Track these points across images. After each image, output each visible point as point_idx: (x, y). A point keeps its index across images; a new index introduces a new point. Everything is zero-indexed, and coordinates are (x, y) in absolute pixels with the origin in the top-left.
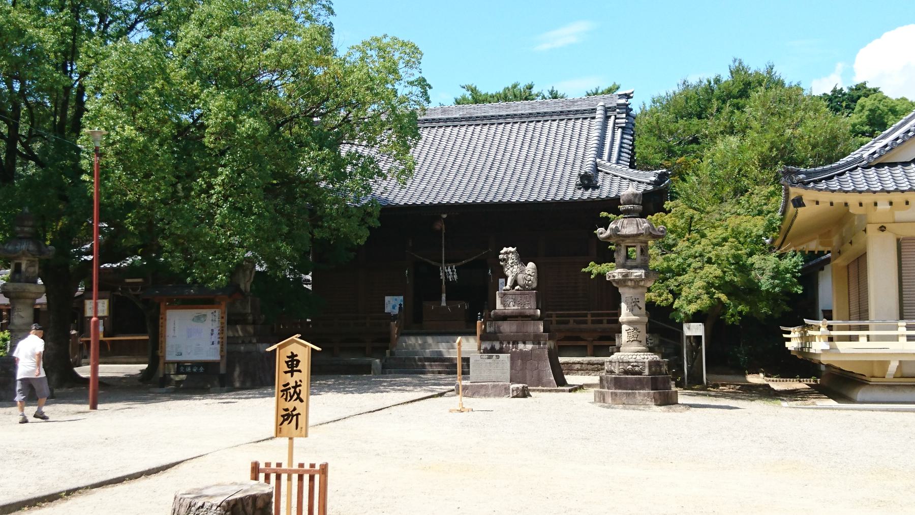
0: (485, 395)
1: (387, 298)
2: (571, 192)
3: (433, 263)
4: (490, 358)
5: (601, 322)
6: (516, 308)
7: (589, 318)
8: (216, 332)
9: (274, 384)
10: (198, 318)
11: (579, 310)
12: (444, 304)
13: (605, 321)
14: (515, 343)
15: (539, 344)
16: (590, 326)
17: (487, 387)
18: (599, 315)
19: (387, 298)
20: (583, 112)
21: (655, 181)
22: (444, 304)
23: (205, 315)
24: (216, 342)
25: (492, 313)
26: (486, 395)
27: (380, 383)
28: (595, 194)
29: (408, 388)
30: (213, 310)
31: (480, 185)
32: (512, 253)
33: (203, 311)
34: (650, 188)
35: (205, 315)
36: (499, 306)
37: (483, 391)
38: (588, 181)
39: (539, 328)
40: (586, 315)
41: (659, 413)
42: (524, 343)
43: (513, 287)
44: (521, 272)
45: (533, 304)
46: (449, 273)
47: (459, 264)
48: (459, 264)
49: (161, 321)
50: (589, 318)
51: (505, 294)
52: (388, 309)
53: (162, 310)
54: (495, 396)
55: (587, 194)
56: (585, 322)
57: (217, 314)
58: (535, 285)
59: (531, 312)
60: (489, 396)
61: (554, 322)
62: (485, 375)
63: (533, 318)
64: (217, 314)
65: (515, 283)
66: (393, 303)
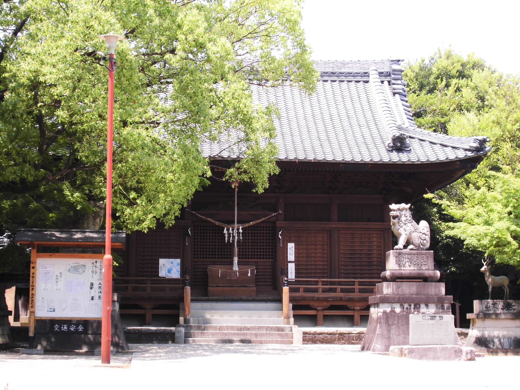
0: (434, 359)
1: (162, 261)
3: (217, 223)
6: (412, 268)
7: (357, 287)
8: (96, 286)
10: (75, 269)
12: (236, 268)
16: (320, 295)
17: (435, 350)
18: (331, 283)
19: (162, 261)
22: (236, 268)
24: (96, 298)
29: (207, 353)
30: (94, 261)
31: (350, 137)
34: (470, 154)
37: (431, 354)
38: (399, 144)
43: (405, 247)
44: (416, 230)
45: (431, 263)
49: (32, 271)
50: (357, 287)
54: (445, 359)
55: (395, 157)
58: (428, 245)
61: (356, 290)
65: (408, 243)
66: (168, 266)
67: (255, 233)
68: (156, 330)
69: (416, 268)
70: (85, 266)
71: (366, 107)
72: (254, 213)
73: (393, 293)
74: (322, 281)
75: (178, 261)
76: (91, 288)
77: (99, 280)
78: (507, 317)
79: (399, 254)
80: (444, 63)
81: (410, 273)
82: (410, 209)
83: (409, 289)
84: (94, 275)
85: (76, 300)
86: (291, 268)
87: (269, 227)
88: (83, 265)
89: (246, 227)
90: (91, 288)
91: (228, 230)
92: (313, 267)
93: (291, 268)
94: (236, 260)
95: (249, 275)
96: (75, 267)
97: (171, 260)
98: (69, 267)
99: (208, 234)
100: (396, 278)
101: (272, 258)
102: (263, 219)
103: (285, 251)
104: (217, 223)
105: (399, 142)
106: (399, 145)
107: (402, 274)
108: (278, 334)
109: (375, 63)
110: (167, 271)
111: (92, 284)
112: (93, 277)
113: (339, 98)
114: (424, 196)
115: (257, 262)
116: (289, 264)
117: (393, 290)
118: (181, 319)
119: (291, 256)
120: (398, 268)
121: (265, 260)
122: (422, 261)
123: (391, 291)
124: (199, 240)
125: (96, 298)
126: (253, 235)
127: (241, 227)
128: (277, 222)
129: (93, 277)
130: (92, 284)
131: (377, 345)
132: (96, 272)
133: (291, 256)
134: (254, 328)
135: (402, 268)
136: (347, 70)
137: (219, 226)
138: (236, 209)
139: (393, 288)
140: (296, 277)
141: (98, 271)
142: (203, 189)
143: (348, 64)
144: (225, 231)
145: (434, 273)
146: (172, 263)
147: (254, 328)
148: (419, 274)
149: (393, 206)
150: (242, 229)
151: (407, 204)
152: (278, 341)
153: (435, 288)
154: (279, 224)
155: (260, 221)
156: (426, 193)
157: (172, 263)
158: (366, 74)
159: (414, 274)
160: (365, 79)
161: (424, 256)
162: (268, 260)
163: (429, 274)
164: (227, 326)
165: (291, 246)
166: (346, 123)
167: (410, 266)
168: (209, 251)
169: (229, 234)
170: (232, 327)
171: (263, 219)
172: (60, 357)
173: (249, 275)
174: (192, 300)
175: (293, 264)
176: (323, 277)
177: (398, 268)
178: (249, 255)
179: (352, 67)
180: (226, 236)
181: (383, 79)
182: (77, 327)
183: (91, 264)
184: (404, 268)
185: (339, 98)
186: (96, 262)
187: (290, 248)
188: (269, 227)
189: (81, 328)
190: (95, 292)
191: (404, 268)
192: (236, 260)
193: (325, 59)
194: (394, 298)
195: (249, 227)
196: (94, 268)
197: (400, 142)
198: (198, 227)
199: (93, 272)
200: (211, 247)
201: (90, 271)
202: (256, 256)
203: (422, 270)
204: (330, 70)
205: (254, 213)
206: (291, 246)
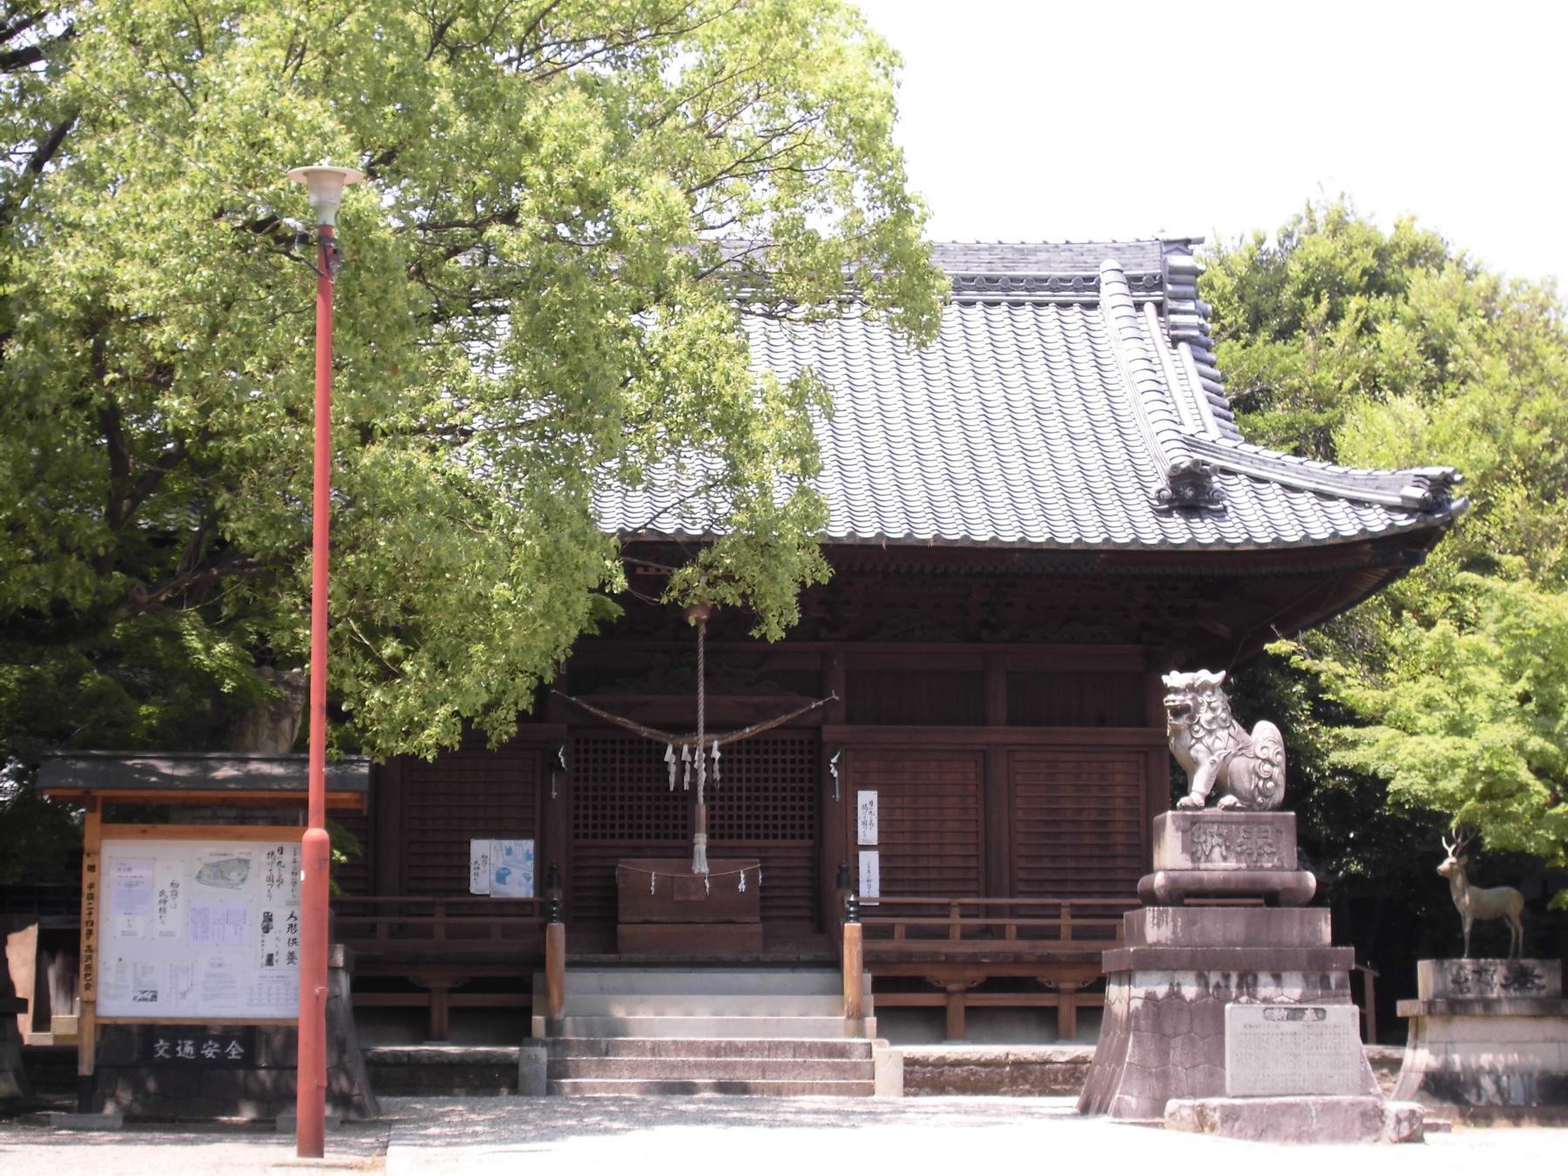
1: (479, 847)
2: (1137, 522)
3: (645, 732)
5: (997, 933)
7: (1066, 922)
8: (280, 923)
10: (217, 873)
12: (701, 866)
16: (955, 946)
17: (1301, 1111)
18: (989, 911)
19: (479, 847)
20: (1057, 285)
21: (1423, 501)
22: (701, 866)
23: (245, 862)
24: (282, 959)
26: (1303, 1136)
27: (434, 1119)
28: (1205, 532)
30: (273, 846)
32: (1213, 688)
33: (238, 849)
34: (1402, 520)
35: (245, 862)
37: (1290, 1124)
38: (1191, 491)
39: (1316, 932)
40: (1055, 912)
42: (1277, 978)
43: (1211, 800)
44: (1242, 750)
45: (1288, 850)
47: (734, 737)
48: (734, 737)
51: (1194, 821)
53: (87, 844)
54: (1333, 1138)
55: (1178, 531)
58: (1279, 795)
60: (1245, 1137)
61: (1065, 932)
65: (1219, 788)
66: (498, 861)
67: (757, 761)
68: (461, 1055)
69: (1243, 865)
70: (246, 861)
71: (1091, 380)
72: (756, 700)
73: (1175, 941)
75: (528, 845)
76: (266, 930)
79: (1193, 823)
81: (1226, 880)
82: (1224, 684)
83: (1223, 927)
85: (220, 965)
86: (869, 865)
88: (240, 860)
89: (731, 744)
90: (266, 930)
91: (677, 751)
92: (933, 862)
93: (869, 865)
94: (701, 842)
95: (742, 886)
96: (217, 865)
97: (506, 843)
98: (198, 867)
100: (1184, 895)
104: (645, 732)
107: (1200, 881)
109: (1118, 249)
110: (493, 877)
111: (268, 918)
112: (270, 896)
113: (1009, 354)
115: (767, 849)
116: (862, 854)
117: (1174, 932)
118: (538, 1020)
119: (868, 832)
120: (1189, 865)
121: (788, 842)
125: (282, 959)
127: (716, 744)
128: (825, 728)
129: (270, 896)
130: (268, 918)
132: (281, 882)
133: (868, 832)
135: (1203, 865)
137: (649, 741)
139: (1175, 926)
140: (882, 892)
143: (1035, 251)
144: (669, 756)
145: (1300, 881)
146: (509, 852)
148: (1253, 881)
149: (1174, 679)
150: (720, 749)
151: (1214, 671)
153: (1302, 923)
154: (829, 733)
155: (773, 724)
156: (1273, 639)
157: (509, 852)
158: (1090, 283)
160: (1088, 297)
162: (797, 842)
164: (675, 1042)
165: (868, 799)
166: (1030, 429)
171: (783, 719)
172: (171, 1136)
173: (742, 886)
174: (571, 965)
176: (966, 893)
177: (1189, 865)
180: (673, 769)
181: (1141, 296)
182: (224, 1045)
183: (264, 858)
184: (1209, 865)
185: (1009, 354)
186: (281, 851)
187: (865, 806)
189: (234, 1050)
190: (278, 941)
191: (1209, 865)
192: (701, 842)
193: (967, 238)
194: (1177, 954)
195: (739, 742)
197: (1194, 486)
199: (270, 880)
201: (264, 877)
203: (1262, 868)
205: (756, 700)
206: (868, 799)
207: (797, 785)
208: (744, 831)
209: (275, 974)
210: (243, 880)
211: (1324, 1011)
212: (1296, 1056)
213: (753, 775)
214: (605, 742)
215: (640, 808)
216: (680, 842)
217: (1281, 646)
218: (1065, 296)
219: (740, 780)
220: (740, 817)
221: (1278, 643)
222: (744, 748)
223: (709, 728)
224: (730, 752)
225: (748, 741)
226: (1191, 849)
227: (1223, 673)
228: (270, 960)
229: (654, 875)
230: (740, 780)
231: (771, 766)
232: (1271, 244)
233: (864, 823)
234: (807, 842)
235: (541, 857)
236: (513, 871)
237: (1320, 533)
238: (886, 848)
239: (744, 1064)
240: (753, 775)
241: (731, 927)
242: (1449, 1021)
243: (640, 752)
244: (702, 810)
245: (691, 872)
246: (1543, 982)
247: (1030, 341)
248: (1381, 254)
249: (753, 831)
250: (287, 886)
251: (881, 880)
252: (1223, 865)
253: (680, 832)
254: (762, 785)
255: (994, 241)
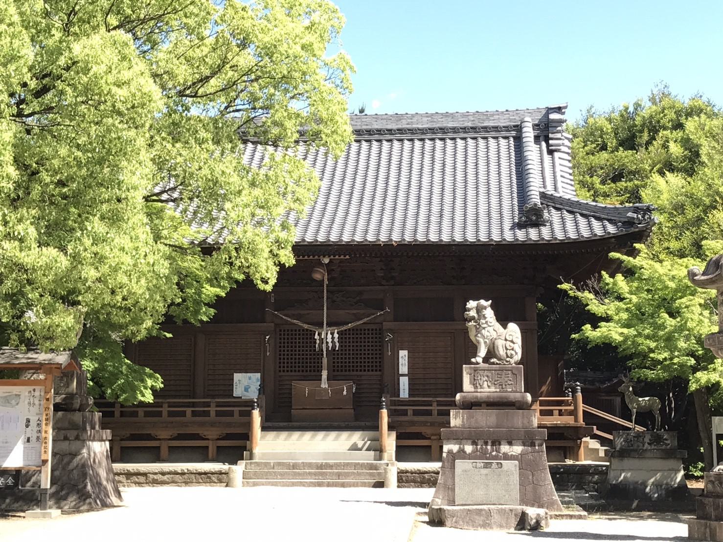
1: (237, 376)
3: (306, 326)
4: (487, 466)
6: (493, 389)
9: (519, 530)
11: (179, 397)
12: (324, 385)
13: (410, 413)
14: (496, 443)
15: (533, 445)
19: (237, 376)
22: (324, 385)
25: (458, 396)
33: (15, 390)
36: (467, 386)
39: (530, 422)
41: (491, 530)
42: (510, 443)
43: (486, 360)
46: (329, 337)
52: (238, 391)
56: (429, 413)
57: (37, 394)
59: (518, 396)
62: (480, 493)
63: (521, 406)
64: (37, 394)
67: (357, 338)
69: (498, 390)
70: (19, 395)
72: (355, 312)
73: (463, 426)
74: (437, 401)
75: (258, 375)
76: (27, 426)
77: (37, 414)
78: (655, 456)
79: (475, 371)
80: (648, 109)
81: (488, 397)
83: (486, 419)
84: (31, 408)
85: (6, 443)
86: (404, 382)
87: (376, 330)
88: (16, 395)
89: (342, 331)
90: (27, 426)
91: (319, 334)
92: (432, 381)
93: (404, 382)
94: (325, 374)
95: (345, 393)
96: (6, 397)
97: (249, 374)
99: (298, 341)
100: (470, 405)
101: (380, 370)
102: (365, 320)
103: (396, 359)
104: (306, 326)
105: (535, 214)
106: (534, 218)
107: (477, 397)
108: (367, 473)
109: (530, 113)
110: (243, 389)
111: (28, 421)
112: (29, 411)
114: (559, 286)
115: (361, 376)
116: (401, 378)
117: (463, 422)
119: (404, 369)
120: (473, 390)
121: (371, 373)
122: (506, 379)
123: (461, 423)
124: (286, 349)
126: (355, 340)
127: (336, 331)
128: (384, 323)
129: (29, 411)
130: (28, 421)
131: (437, 500)
132: (34, 404)
133: (404, 369)
134: (338, 466)
135: (479, 390)
136: (491, 124)
137: (307, 330)
138: (325, 308)
139: (463, 419)
140: (410, 395)
141: (37, 402)
142: (635, 248)
143: (493, 115)
144: (317, 337)
145: (523, 397)
146: (250, 378)
147: (338, 466)
148: (501, 398)
150: (338, 333)
151: (487, 300)
152: (365, 483)
153: (523, 418)
154: (386, 325)
155: (361, 322)
156: (561, 283)
157: (250, 378)
159: (494, 398)
161: (510, 372)
162: (374, 373)
163: (515, 398)
164: (303, 463)
165: (403, 354)
167: (489, 386)
168: (299, 363)
169: (321, 340)
170: (310, 463)
171: (365, 320)
173: (345, 393)
175: (407, 378)
176: (440, 395)
177: (473, 390)
178: (365, 366)
179: (499, 118)
180: (318, 342)
183: (27, 394)
184: (482, 390)
186: (34, 390)
187: (402, 357)
188: (376, 330)
191: (482, 390)
192: (325, 374)
194: (462, 432)
195: (346, 330)
196: (32, 399)
197: (535, 214)
198: (284, 331)
199: (29, 403)
200: (301, 357)
201: (26, 402)
202: (359, 368)
203: (507, 392)
204: (470, 124)
205: (355, 312)
206: (403, 354)
207: (374, 348)
208: (351, 368)
209: (31, 446)
210: (17, 404)
211: (501, 464)
212: (487, 486)
213: (355, 344)
214: (292, 331)
215: (307, 359)
216: (318, 374)
217: (565, 286)
218: (504, 134)
219: (349, 346)
220: (349, 362)
221: (563, 285)
222: (351, 332)
223: (329, 325)
224: (342, 334)
225: (349, 330)
226: (474, 382)
227: (490, 301)
228: (28, 440)
229: (305, 388)
230: (349, 346)
231: (359, 340)
232: (631, 109)
233: (402, 365)
234: (379, 373)
235: (263, 379)
236: (252, 386)
237: (586, 233)
238: (411, 375)
239: (330, 473)
240: (355, 344)
241: (340, 410)
242: (622, 460)
243: (307, 334)
244: (325, 360)
245: (231, 396)
246: (668, 442)
247: (438, 154)
248: (678, 113)
249: (355, 369)
250: (37, 407)
251: (409, 389)
252: (487, 390)
253: (316, 369)
254: (359, 348)
255: (474, 111)
